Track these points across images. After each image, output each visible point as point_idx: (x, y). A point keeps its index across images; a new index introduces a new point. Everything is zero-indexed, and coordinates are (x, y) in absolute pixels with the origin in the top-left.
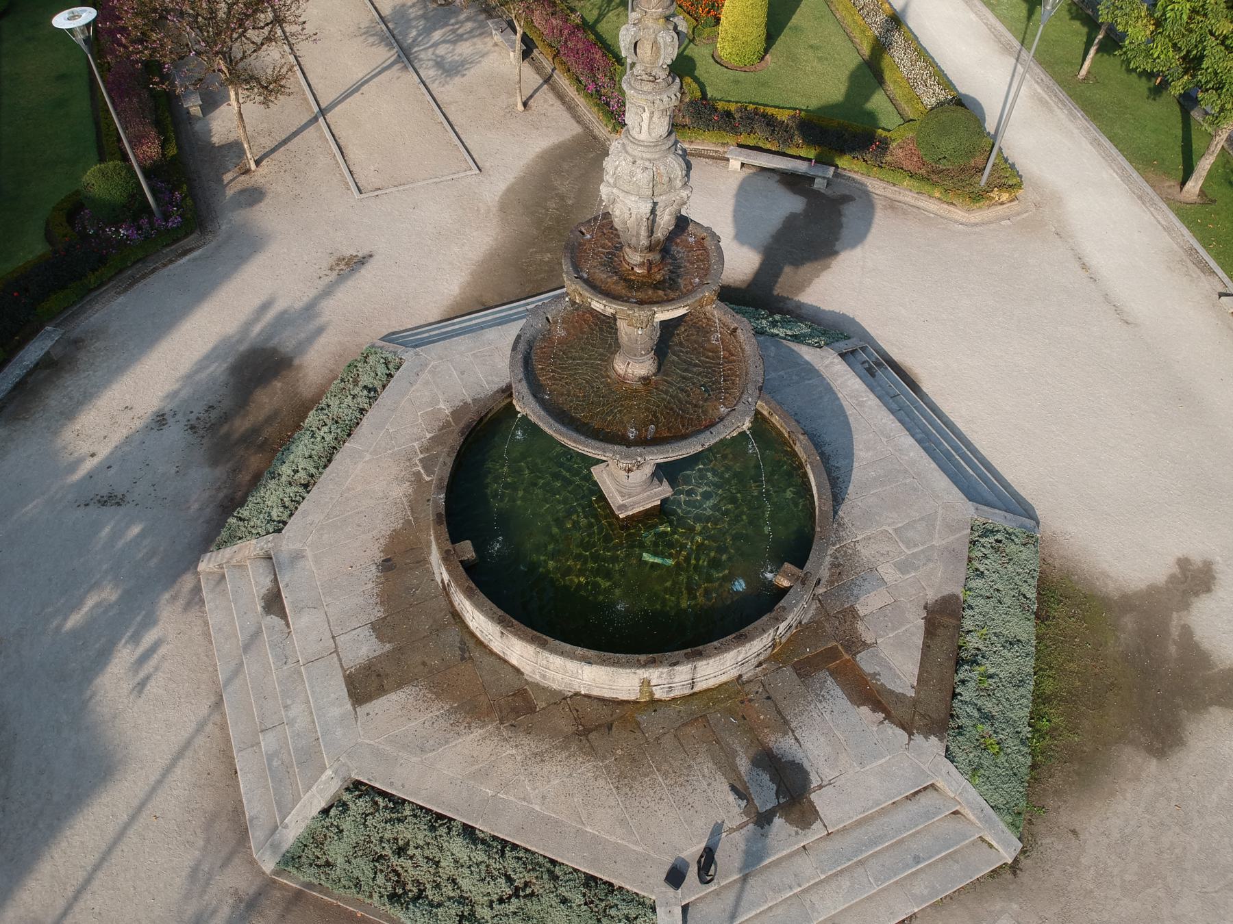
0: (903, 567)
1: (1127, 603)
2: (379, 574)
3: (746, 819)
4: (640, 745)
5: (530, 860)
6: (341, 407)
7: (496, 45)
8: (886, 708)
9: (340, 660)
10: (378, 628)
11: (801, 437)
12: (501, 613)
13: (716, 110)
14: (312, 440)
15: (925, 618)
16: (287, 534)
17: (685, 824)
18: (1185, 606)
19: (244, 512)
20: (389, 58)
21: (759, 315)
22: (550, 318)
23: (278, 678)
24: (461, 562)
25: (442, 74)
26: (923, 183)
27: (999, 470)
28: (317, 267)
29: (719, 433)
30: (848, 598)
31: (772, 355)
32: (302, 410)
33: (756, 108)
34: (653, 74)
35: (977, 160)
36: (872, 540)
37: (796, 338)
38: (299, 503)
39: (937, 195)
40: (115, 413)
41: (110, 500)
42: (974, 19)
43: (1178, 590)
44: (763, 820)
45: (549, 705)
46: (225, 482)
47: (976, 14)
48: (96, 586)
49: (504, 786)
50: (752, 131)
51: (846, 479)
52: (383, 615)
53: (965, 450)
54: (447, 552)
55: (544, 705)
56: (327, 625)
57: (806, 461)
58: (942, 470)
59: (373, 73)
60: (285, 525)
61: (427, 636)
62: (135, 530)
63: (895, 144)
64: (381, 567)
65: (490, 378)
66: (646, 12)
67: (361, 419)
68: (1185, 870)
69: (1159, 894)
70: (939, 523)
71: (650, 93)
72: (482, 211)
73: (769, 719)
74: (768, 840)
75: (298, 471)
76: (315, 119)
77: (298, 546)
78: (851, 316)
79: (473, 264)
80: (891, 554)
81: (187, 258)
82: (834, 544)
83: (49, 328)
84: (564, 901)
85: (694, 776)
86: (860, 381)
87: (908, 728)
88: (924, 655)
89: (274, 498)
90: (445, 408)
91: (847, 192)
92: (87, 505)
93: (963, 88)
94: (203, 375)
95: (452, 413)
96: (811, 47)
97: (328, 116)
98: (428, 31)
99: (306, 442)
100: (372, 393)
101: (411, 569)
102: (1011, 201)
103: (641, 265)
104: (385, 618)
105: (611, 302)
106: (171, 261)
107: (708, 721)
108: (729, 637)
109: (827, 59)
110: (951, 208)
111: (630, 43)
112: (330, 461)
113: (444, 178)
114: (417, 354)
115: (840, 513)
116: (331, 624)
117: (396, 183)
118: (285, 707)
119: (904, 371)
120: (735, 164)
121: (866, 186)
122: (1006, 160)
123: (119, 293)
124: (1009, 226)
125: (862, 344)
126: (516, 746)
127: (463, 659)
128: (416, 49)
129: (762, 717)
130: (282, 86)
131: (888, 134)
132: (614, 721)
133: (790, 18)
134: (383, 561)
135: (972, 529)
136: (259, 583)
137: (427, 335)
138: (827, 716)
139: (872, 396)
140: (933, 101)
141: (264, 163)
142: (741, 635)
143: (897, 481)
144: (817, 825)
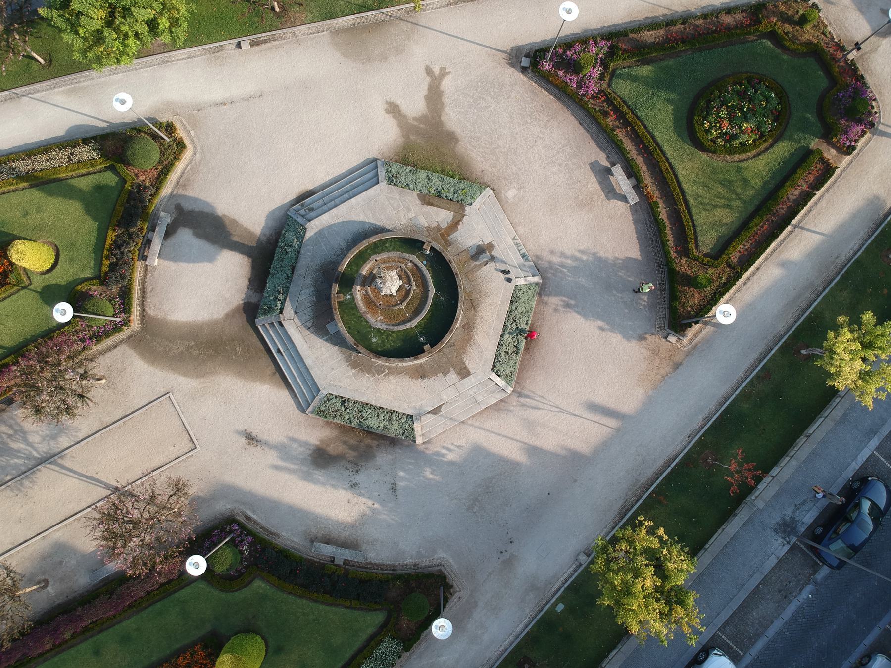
0: (409, 210)
1: (406, 135)
5: (507, 319)
10: (445, 374)
18: (404, 116)
41: (394, 488)
44: (492, 258)
49: (490, 327)
54: (428, 353)
62: (402, 474)
84: (516, 308)
90: (353, 371)
95: (355, 368)
115: (389, 228)
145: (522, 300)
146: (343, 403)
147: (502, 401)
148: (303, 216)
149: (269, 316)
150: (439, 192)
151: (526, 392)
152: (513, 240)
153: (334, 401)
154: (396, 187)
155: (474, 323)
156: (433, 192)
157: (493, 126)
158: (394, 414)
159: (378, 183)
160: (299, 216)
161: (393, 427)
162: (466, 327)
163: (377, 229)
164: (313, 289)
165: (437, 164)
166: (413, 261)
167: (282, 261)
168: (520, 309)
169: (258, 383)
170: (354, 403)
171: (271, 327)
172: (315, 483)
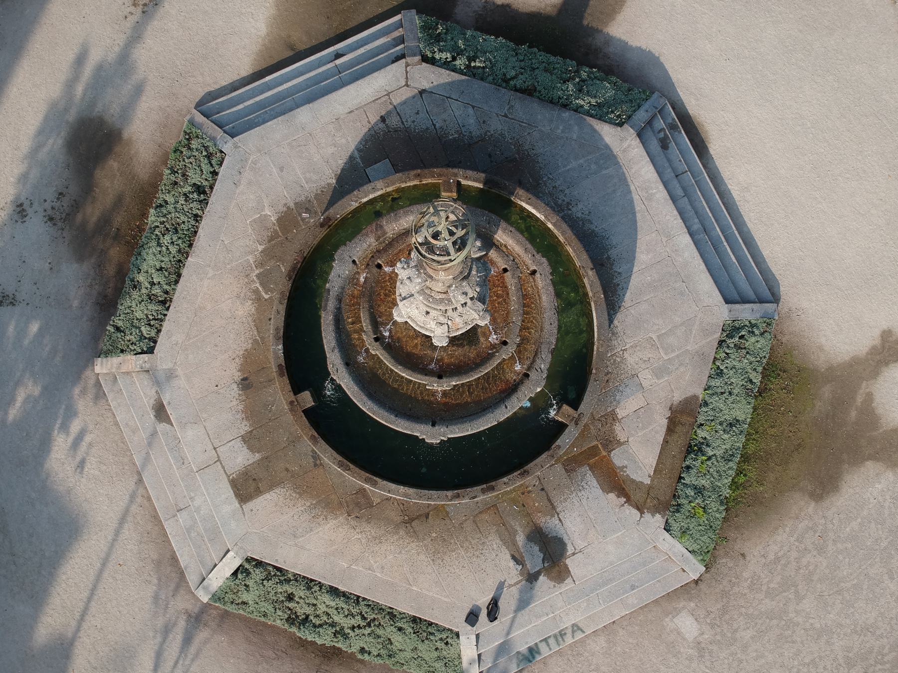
0: (659, 373)
2: (240, 392)
3: (521, 578)
4: (448, 529)
5: (374, 607)
8: (627, 494)
9: (223, 467)
10: (248, 440)
11: (590, 273)
12: (340, 458)
15: (669, 417)
17: (479, 583)
18: (875, 374)
22: (356, 260)
27: (759, 244)
30: (611, 403)
36: (638, 348)
38: (162, 320)
43: (873, 361)
44: (532, 578)
45: (383, 501)
46: (95, 279)
49: (356, 560)
51: (625, 286)
52: (248, 429)
55: (379, 501)
56: (208, 439)
61: (287, 447)
62: (34, 327)
65: (308, 175)
68: (812, 581)
69: (790, 596)
73: (542, 506)
74: (534, 592)
78: (657, 55)
80: (651, 360)
84: (400, 629)
85: (486, 550)
87: (640, 509)
88: (662, 449)
94: (43, 154)
101: (265, 387)
104: (251, 432)
107: (498, 509)
108: (515, 474)
112: (179, 276)
115: (616, 322)
116: (211, 437)
118: (190, 499)
126: (361, 532)
127: (315, 465)
129: (536, 505)
132: (430, 511)
134: (242, 380)
136: (146, 394)
138: (584, 502)
142: (525, 471)
144: (569, 580)
145: (420, 646)
146: (199, 189)
147: (182, 575)
148: (650, 123)
149: (420, 35)
150: (700, 450)
151: (202, 635)
152: (573, 625)
153: (206, 168)
154: (716, 345)
155: (368, 521)
156: (702, 433)
157: (849, 585)
158: (160, 308)
159: (727, 301)
160: (650, 114)
161: (134, 305)
162: (362, 501)
163: (614, 292)
164: (476, 132)
165: (763, 445)
166: (527, 383)
167: (546, 70)
168: (398, 639)
169: (273, 11)
170: (196, 216)
171: (394, 39)
172: (40, 132)
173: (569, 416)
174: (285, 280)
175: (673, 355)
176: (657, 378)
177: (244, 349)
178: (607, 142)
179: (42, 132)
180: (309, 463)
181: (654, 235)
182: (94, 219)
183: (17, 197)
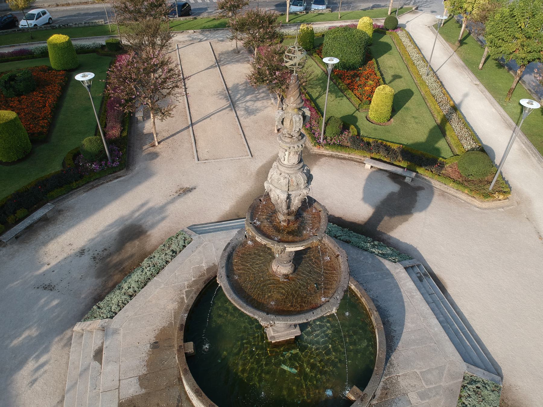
0: (423, 396)
2: (150, 350)
6: (158, 259)
7: (272, 104)
9: (119, 393)
10: (143, 380)
11: (375, 313)
12: (197, 387)
13: (363, 141)
14: (141, 273)
16: (115, 320)
19: (101, 304)
20: (226, 105)
21: (367, 240)
22: (247, 235)
23: (89, 396)
24: (186, 353)
25: (246, 114)
26: (460, 185)
28: (170, 191)
29: (317, 314)
31: (370, 262)
32: (146, 255)
33: (382, 142)
34: (291, 134)
35: (489, 177)
36: (407, 377)
37: (384, 256)
39: (466, 192)
40: (64, 246)
41: (49, 287)
42: (494, 111)
47: (496, 109)
48: (29, 328)
50: (379, 152)
51: (398, 338)
52: (145, 372)
53: (467, 330)
54: (180, 346)
57: (376, 327)
58: (451, 341)
59: (217, 111)
60: (116, 315)
61: (164, 389)
62: (55, 303)
63: (448, 165)
64: (152, 346)
66: (288, 105)
67: (165, 266)
70: (446, 372)
71: (289, 143)
72: (249, 174)
75: (130, 288)
76: (188, 127)
77: (118, 327)
78: (415, 247)
79: (238, 198)
80: (416, 386)
81: (117, 180)
82: (386, 376)
83: (49, 204)
86: (413, 284)
89: (116, 300)
91: (421, 185)
92: (38, 288)
93: (485, 142)
95: (207, 269)
96: (413, 117)
97: (194, 127)
98: (245, 96)
99: (138, 273)
100: (174, 254)
101: (166, 349)
102: (504, 199)
103: (284, 221)
104: (146, 374)
105: (264, 239)
106: (111, 181)
109: (420, 123)
110: (473, 199)
111: (279, 119)
112: (145, 285)
113: (236, 158)
114: (199, 238)
117: (214, 158)
119: (439, 280)
120: (368, 166)
121: (431, 183)
122: (504, 179)
123: (85, 192)
124: (503, 212)
125: (418, 263)
128: (238, 103)
130: (170, 114)
131: (445, 160)
133: (405, 104)
134: (154, 343)
135: (464, 378)
137: (208, 228)
139: (419, 293)
140: (469, 147)
141: (162, 143)
143: (426, 344)
163: (392, 340)
172: (109, 226)
173: (357, 394)
174: (202, 284)
175: (431, 386)
176: (421, 399)
177: (163, 326)
178: (387, 267)
179: (111, 226)
180: (174, 404)
181: (415, 315)
182: (114, 262)
183: (84, 246)
